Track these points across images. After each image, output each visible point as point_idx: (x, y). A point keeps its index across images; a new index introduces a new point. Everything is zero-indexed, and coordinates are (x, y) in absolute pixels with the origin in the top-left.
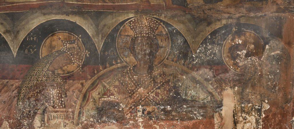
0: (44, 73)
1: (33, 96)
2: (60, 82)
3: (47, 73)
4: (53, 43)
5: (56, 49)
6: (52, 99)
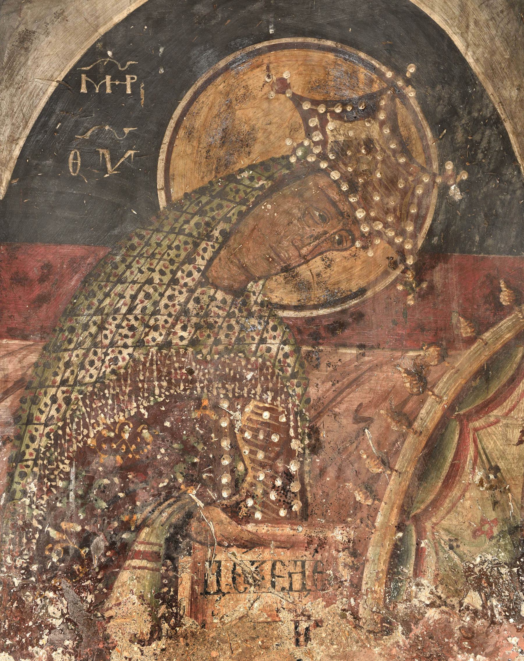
0: (182, 299)
1: (109, 440)
2: (280, 356)
3: (197, 300)
4: (239, 113)
5: (257, 148)
6: (226, 462)
